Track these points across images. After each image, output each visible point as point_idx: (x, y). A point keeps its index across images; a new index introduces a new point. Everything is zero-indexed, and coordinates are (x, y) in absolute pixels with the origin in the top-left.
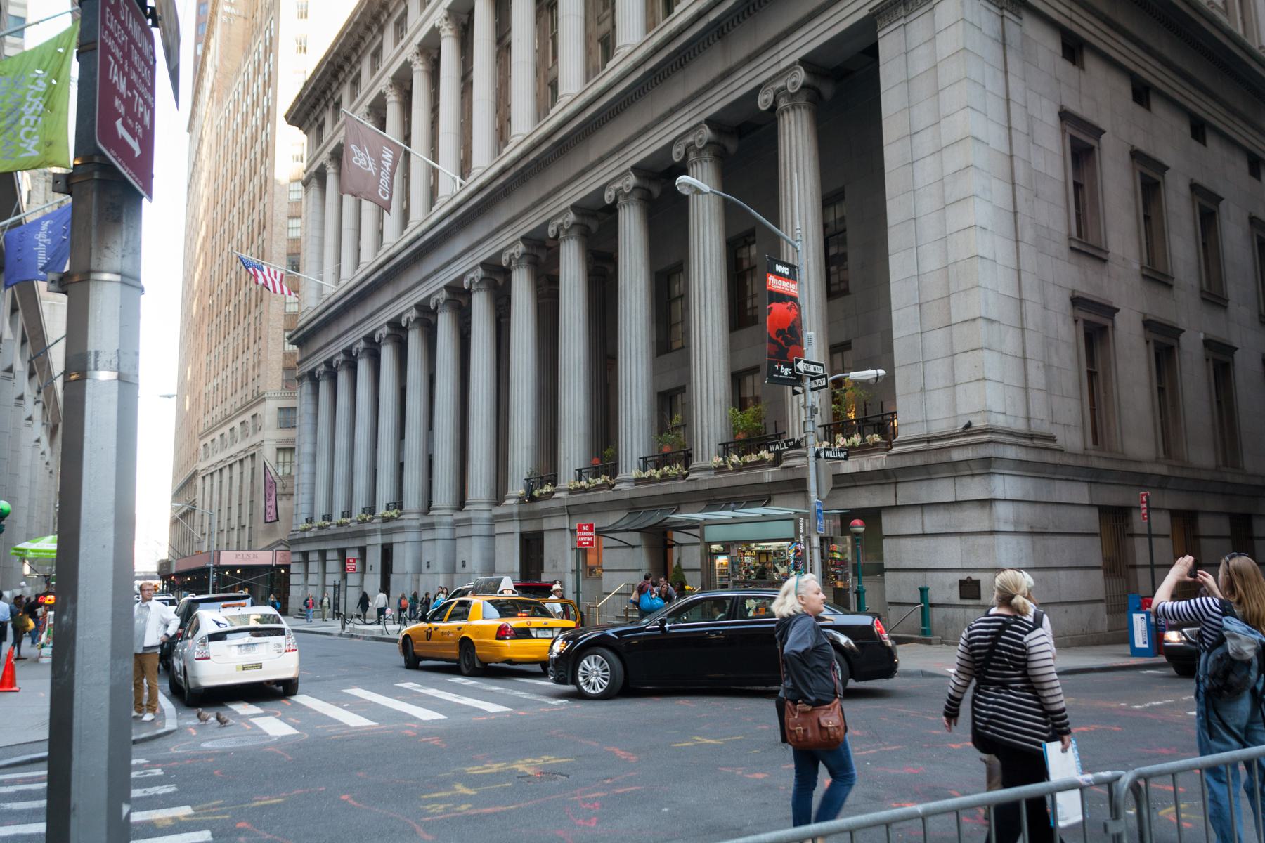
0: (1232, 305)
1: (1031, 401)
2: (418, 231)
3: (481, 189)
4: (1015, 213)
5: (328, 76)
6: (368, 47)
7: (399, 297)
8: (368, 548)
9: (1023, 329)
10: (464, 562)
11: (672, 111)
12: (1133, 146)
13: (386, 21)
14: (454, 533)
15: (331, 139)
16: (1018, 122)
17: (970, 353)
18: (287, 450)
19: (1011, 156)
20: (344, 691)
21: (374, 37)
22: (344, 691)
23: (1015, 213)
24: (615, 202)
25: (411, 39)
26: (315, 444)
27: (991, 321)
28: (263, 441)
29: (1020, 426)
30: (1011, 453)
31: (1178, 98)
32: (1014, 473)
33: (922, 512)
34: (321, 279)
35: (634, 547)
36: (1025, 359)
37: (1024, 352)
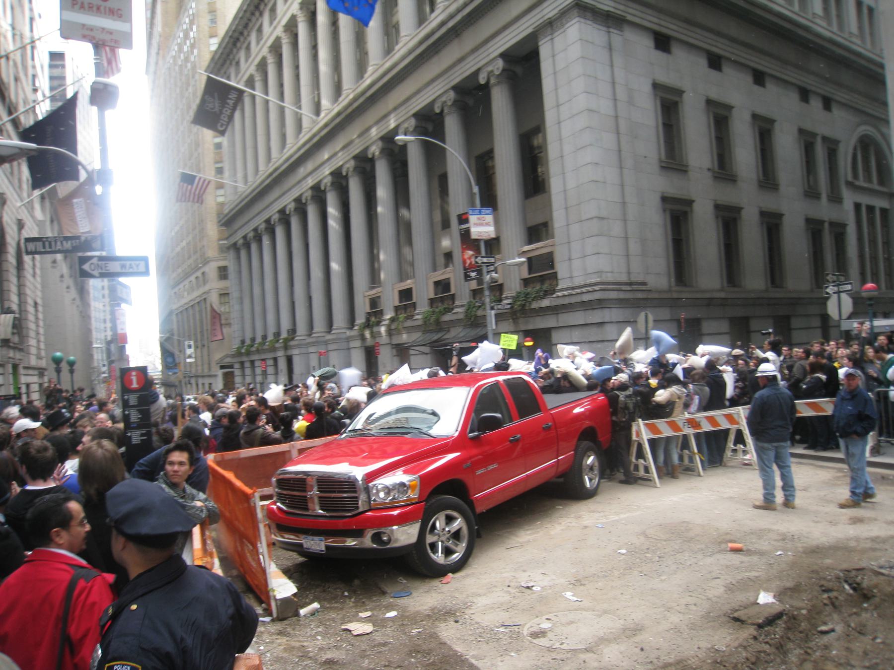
0: (783, 188)
3: (326, 125)
4: (620, 151)
5: (230, 45)
6: (254, 26)
7: (284, 194)
11: (433, 81)
13: (264, 9)
15: (257, 55)
16: (621, 94)
18: (224, 295)
20: (458, 454)
21: (257, 19)
22: (458, 454)
23: (620, 151)
24: (442, 111)
25: (279, 22)
26: (241, 291)
27: (603, 218)
28: (210, 290)
29: (624, 278)
30: (613, 295)
31: (743, 61)
34: (236, 182)
35: (427, 354)
37: (626, 233)
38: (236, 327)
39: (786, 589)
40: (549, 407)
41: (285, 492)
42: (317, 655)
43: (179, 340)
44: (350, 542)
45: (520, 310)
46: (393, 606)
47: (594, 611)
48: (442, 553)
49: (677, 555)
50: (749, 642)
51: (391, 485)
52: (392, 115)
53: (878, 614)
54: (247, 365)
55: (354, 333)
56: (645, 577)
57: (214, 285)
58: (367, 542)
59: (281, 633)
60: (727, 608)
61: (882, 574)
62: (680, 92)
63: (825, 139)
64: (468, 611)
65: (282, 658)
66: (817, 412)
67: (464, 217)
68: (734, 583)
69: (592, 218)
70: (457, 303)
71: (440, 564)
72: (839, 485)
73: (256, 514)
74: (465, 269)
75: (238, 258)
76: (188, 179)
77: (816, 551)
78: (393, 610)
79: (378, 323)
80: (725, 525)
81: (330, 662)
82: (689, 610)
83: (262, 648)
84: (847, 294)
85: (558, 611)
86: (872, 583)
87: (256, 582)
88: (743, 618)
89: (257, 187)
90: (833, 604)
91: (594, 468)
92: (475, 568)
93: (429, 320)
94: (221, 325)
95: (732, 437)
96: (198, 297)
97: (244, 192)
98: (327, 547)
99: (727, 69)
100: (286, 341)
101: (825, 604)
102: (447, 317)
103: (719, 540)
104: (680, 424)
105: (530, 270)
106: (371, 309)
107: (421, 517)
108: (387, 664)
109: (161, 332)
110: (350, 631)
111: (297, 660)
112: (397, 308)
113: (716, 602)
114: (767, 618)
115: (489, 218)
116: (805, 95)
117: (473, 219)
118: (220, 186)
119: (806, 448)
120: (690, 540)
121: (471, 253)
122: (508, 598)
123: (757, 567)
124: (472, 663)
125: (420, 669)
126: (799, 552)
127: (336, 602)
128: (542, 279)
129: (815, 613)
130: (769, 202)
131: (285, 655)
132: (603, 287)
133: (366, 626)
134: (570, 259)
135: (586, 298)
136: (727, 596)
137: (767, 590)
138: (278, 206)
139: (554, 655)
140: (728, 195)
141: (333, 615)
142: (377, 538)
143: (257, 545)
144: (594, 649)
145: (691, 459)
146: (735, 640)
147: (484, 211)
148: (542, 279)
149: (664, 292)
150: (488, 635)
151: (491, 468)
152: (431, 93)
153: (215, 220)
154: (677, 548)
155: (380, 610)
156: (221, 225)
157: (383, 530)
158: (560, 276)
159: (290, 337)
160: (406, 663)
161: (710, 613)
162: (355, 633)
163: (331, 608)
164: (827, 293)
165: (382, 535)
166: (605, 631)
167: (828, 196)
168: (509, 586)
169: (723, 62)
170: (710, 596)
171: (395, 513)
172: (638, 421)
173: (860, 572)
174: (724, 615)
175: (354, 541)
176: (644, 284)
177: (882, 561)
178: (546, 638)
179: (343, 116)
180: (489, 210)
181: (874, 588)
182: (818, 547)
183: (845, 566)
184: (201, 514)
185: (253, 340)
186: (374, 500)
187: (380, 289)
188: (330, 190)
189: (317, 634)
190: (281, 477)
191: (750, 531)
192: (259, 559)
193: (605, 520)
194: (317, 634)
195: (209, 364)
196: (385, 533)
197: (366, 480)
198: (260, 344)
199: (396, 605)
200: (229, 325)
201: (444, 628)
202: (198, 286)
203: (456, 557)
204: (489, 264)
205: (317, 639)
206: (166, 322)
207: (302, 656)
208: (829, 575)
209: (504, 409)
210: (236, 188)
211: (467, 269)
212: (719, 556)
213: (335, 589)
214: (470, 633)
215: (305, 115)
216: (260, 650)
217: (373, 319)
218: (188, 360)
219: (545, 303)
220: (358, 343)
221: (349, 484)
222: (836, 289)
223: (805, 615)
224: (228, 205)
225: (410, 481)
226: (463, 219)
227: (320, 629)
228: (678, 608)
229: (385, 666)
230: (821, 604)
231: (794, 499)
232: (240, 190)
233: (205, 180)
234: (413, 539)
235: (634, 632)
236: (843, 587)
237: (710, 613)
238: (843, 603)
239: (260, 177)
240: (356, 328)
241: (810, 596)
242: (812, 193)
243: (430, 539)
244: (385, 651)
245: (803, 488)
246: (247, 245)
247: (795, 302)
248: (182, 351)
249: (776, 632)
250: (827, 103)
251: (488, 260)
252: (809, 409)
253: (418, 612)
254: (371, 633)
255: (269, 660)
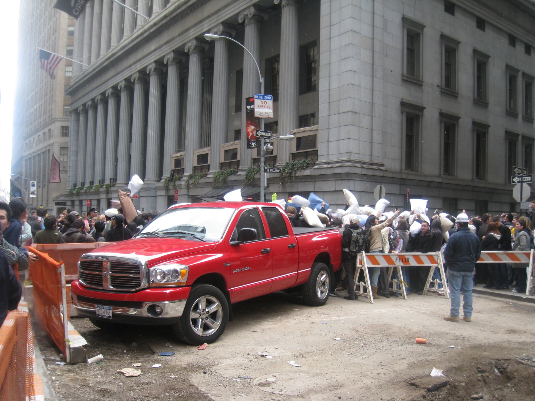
0: (491, 106)
1: (373, 148)
2: (127, 42)
3: (155, 24)
4: (373, 64)
8: (101, 200)
9: (372, 116)
10: (102, 209)
12: (442, 32)
14: (156, 194)
16: (378, 22)
17: (345, 127)
18: (64, 148)
19: (373, 39)
23: (373, 64)
24: (244, 22)
27: (356, 113)
28: (53, 143)
29: (367, 159)
30: (358, 171)
31: (470, 10)
32: (361, 180)
33: (324, 195)
34: (82, 61)
36: (372, 130)
38: (71, 173)
39: (452, 368)
40: (295, 234)
41: (86, 272)
42: (95, 386)
43: (26, 180)
44: (132, 312)
45: (288, 176)
46: (158, 361)
47: (309, 373)
48: (201, 327)
49: (378, 344)
50: (419, 399)
51: (166, 271)
52: (206, 22)
53: (515, 389)
54: (77, 203)
55: (160, 184)
56: (351, 355)
57: (57, 140)
58: (144, 312)
59: (70, 371)
60: (407, 377)
61: (522, 364)
62: (422, 27)
63: (524, 74)
64: (215, 368)
65: (68, 385)
66: (495, 261)
67: (251, 100)
68: (415, 362)
69: (347, 112)
70: (240, 168)
71: (198, 335)
72: (504, 311)
73: (61, 281)
74: (248, 139)
75: (78, 120)
76: (44, 55)
77: (480, 347)
78: (159, 363)
79: (180, 179)
80: (415, 328)
81: (104, 392)
82: (380, 377)
83: (54, 378)
84: (527, 183)
85: (283, 372)
86: (514, 369)
87: (57, 337)
88: (418, 384)
89: (97, 67)
90: (485, 381)
91: (326, 283)
92: (226, 342)
93: (219, 179)
94: (60, 171)
95: (432, 273)
96: (44, 148)
97: (88, 70)
98: (114, 315)
99: (458, 14)
100: (108, 187)
101: (479, 380)
102: (232, 178)
103: (410, 337)
104: (394, 259)
105: (298, 148)
106: (175, 167)
107: (187, 297)
108: (147, 395)
109: (12, 172)
110: (123, 374)
111: (79, 387)
112: (195, 168)
113: (400, 373)
114: (435, 385)
115: (270, 103)
116: (513, 41)
117: (257, 102)
118: (69, 64)
119: (484, 287)
120: (388, 335)
121: (253, 127)
122: (247, 361)
123: (434, 354)
124: (211, 399)
125: (171, 400)
126: (467, 347)
127: (117, 357)
128: (306, 155)
129: (470, 385)
130: (480, 116)
131: (70, 383)
132: (351, 164)
133: (136, 371)
134: (328, 141)
135: (338, 171)
136: (409, 370)
137: (438, 368)
138: (112, 83)
139: (273, 398)
140: (450, 107)
141: (113, 363)
142: (152, 309)
143: (59, 305)
144: (304, 396)
145: (399, 287)
146: (409, 396)
147: (267, 97)
148: (306, 155)
149: (397, 173)
150: (227, 383)
151: (245, 269)
152: (237, 7)
153: (63, 90)
154: (378, 339)
155: (149, 363)
156: (66, 94)
157: (157, 303)
158: (319, 153)
159: (112, 184)
160: (162, 396)
161: (394, 379)
162: (127, 375)
163: (112, 360)
164: (514, 182)
165: (156, 308)
166: (315, 385)
167: (523, 117)
168: (249, 354)
169: (456, 8)
170: (396, 369)
171: (168, 291)
172: (362, 253)
173: (507, 361)
174: (404, 382)
175: (135, 311)
176: (382, 165)
177: (524, 356)
178: (270, 387)
179: (169, 18)
180: (271, 97)
181: (515, 372)
182: (480, 345)
183: (497, 357)
184: (12, 257)
185: (83, 184)
186: (153, 281)
187: (183, 153)
188: (153, 74)
189: (98, 374)
190: (85, 260)
191: (434, 333)
192: (60, 316)
193: (328, 320)
194: (98, 374)
195: (47, 201)
196: (158, 306)
197: (147, 265)
198: (88, 188)
199: (162, 360)
200: (66, 171)
201: (194, 376)
202: (45, 140)
203: (211, 332)
204: (266, 138)
205: (98, 377)
206: (17, 166)
207: (83, 385)
208: (484, 362)
209: (259, 225)
210: (81, 66)
211: (250, 140)
212: (408, 346)
213: (117, 348)
214: (214, 380)
215: (140, 15)
216: (52, 379)
217: (176, 176)
218: (31, 196)
219: (307, 172)
220: (163, 193)
221: (135, 267)
222: (520, 179)
223: (463, 386)
224: (73, 79)
225: (182, 269)
226: (250, 102)
227: (101, 372)
228: (372, 375)
229: (146, 396)
230: (476, 380)
231: (471, 315)
232: (84, 68)
233: (58, 57)
234: (180, 314)
235: (336, 388)
236: (494, 370)
237: (394, 379)
238: (492, 381)
239: (101, 60)
240: (163, 181)
241: (469, 374)
242: (511, 113)
243: (193, 315)
244: (148, 388)
245: (478, 311)
246: (86, 112)
247: (493, 192)
248: (27, 189)
249: (440, 394)
250: (528, 50)
251: (266, 134)
252: (489, 257)
253: (177, 366)
254: (139, 376)
255: (58, 386)
